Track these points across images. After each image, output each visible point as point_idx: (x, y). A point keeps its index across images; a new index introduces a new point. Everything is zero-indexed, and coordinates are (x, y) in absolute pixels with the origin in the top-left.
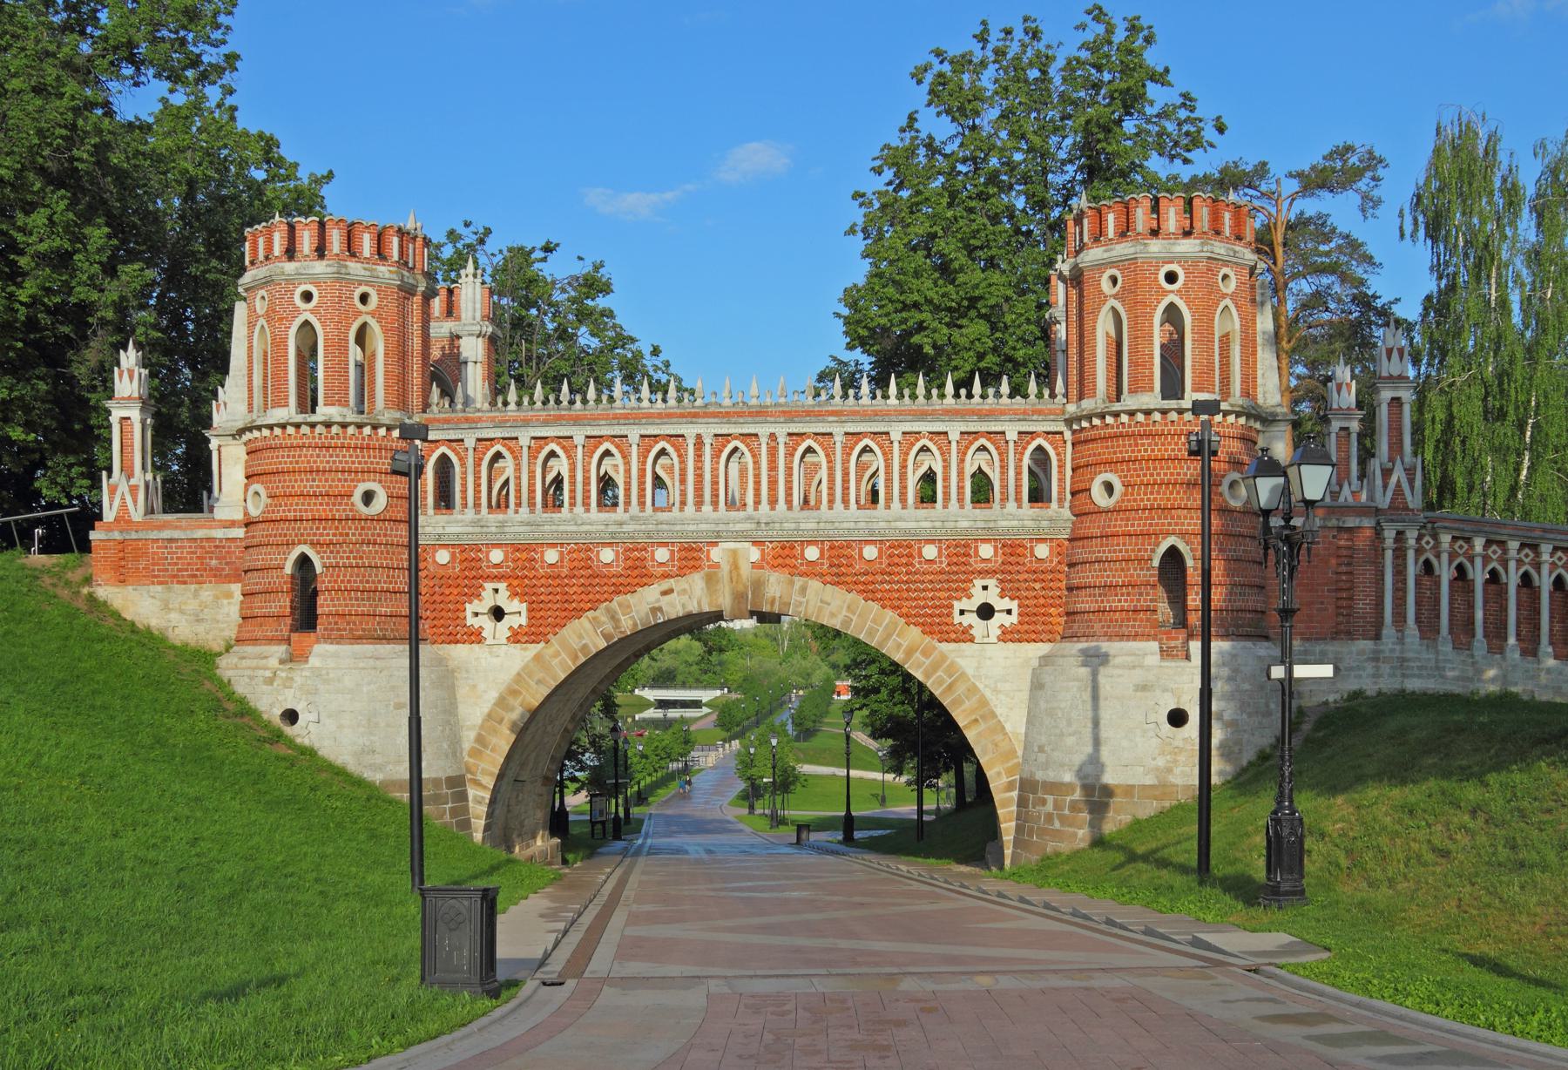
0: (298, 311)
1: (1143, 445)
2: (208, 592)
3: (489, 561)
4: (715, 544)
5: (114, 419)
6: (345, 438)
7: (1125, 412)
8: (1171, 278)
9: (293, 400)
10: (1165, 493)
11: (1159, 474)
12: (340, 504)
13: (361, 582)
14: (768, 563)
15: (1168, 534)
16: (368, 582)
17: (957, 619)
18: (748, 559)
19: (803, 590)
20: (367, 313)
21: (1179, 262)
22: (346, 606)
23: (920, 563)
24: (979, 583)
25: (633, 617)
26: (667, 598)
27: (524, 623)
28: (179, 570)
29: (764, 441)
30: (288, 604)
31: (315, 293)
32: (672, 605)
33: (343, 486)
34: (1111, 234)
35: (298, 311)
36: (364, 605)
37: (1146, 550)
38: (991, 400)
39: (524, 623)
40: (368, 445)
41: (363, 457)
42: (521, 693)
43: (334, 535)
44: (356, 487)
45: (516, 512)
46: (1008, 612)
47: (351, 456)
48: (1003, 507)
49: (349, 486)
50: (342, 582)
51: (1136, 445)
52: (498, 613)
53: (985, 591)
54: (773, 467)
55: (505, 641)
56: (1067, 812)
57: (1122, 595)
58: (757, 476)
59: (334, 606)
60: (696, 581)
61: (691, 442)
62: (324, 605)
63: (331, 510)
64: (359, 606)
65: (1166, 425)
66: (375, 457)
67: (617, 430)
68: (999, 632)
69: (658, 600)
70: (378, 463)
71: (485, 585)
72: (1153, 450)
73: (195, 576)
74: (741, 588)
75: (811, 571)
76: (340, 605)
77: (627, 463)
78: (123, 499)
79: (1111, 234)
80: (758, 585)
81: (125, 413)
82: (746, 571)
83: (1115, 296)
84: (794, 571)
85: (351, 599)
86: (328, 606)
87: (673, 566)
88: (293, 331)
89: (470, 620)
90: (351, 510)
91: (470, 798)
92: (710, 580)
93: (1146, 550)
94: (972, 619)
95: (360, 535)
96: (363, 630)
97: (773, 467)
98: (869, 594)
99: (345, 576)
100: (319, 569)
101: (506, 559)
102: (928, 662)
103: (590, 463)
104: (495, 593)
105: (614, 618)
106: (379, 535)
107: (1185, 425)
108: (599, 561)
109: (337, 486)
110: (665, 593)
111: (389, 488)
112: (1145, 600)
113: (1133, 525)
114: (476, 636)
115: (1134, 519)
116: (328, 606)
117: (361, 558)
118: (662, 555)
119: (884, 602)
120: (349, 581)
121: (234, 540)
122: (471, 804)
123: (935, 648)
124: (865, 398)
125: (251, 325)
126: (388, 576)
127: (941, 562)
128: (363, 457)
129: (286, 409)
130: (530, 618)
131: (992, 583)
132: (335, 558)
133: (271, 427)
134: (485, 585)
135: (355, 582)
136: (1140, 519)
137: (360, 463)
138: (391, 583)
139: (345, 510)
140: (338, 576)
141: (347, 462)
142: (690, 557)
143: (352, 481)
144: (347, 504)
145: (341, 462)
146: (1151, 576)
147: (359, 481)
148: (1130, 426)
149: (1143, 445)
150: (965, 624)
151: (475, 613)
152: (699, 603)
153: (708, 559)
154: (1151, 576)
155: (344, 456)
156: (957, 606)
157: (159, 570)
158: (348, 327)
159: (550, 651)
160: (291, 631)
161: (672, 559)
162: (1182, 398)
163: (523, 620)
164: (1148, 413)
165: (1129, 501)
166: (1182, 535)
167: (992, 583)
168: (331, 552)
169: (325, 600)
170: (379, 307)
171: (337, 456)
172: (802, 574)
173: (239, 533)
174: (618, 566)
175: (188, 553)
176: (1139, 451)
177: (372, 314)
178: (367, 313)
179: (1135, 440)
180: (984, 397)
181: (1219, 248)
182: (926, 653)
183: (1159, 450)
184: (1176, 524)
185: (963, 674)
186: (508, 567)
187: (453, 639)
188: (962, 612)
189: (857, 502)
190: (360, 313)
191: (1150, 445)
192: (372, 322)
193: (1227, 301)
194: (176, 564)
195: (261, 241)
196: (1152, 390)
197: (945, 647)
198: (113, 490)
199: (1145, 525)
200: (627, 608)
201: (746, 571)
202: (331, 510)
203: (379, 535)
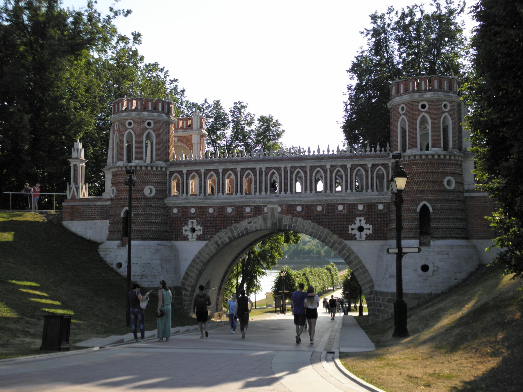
0: (127, 129)
1: (413, 168)
2: (99, 222)
3: (190, 212)
4: (266, 206)
5: (72, 165)
6: (141, 171)
7: (407, 156)
8: (423, 106)
9: (125, 158)
10: (421, 185)
11: (419, 178)
12: (139, 193)
13: (146, 219)
14: (284, 212)
15: (422, 201)
16: (148, 219)
17: (350, 232)
18: (277, 211)
19: (296, 222)
20: (150, 129)
21: (426, 101)
22: (140, 227)
23: (337, 212)
24: (358, 219)
25: (238, 231)
26: (250, 225)
27: (202, 234)
28: (90, 215)
29: (283, 169)
30: (121, 227)
31: (133, 125)
32: (251, 227)
33: (140, 187)
34: (402, 91)
35: (127, 129)
36: (147, 228)
37: (415, 206)
38: (373, 152)
39: (202, 234)
40: (149, 173)
41: (147, 177)
42: (200, 258)
43: (137, 203)
44: (145, 187)
45: (236, 194)
46: (368, 229)
47: (143, 177)
48: (366, 191)
49: (142, 187)
50: (139, 219)
51: (411, 168)
52: (361, 229)
53: (360, 221)
54: (286, 178)
55: (364, 240)
56: (386, 303)
57: (407, 223)
58: (255, 181)
59: (136, 228)
60: (260, 218)
61: (283, 169)
62: (134, 227)
63: (136, 195)
64: (145, 228)
65: (422, 160)
66: (152, 177)
67: (233, 167)
68: (365, 237)
69: (247, 225)
70: (152, 179)
71: (189, 220)
72: (417, 170)
73: (95, 217)
74: (275, 221)
75: (299, 215)
76: (138, 227)
77: (280, 177)
78: (74, 192)
79: (402, 91)
80: (281, 220)
81: (75, 163)
82: (277, 215)
83: (403, 114)
84: (294, 215)
85: (142, 225)
86: (134, 228)
87: (252, 213)
88: (125, 136)
89: (184, 232)
90: (143, 195)
91: (183, 294)
92: (265, 219)
93: (415, 206)
94: (356, 232)
95: (146, 203)
96: (146, 236)
97: (286, 178)
98: (319, 223)
99: (140, 217)
100: (431, 210)
101: (196, 212)
102: (340, 247)
103: (373, 174)
104: (192, 223)
105: (231, 231)
106: (153, 203)
107: (411, 161)
108: (227, 212)
109: (138, 187)
110: (249, 223)
111: (156, 187)
112: (415, 225)
113: (410, 197)
114: (353, 238)
115: (411, 195)
116: (134, 228)
117: (146, 211)
118: (248, 210)
119: (325, 226)
120: (142, 219)
121: (108, 205)
122: (183, 297)
123: (343, 242)
124: (368, 151)
125: (114, 133)
126: (155, 217)
127: (345, 211)
128: (147, 177)
129: (123, 162)
130: (203, 232)
131: (362, 218)
132: (137, 211)
133: (118, 167)
134: (189, 220)
135: (144, 219)
136: (413, 195)
137: (146, 179)
138: (156, 220)
139: (141, 195)
140: (138, 217)
141: (142, 179)
142: (258, 210)
143: (144, 185)
144: (142, 193)
145: (140, 179)
146: (417, 215)
147: (146, 185)
148: (409, 161)
149: (413, 168)
150: (353, 234)
151: (186, 230)
152: (261, 226)
153: (264, 211)
154: (417, 215)
155: (141, 177)
156: (350, 227)
157: (84, 216)
158: (143, 134)
159: (211, 243)
160: (122, 236)
161: (251, 211)
162: (398, 150)
163: (201, 233)
164: (415, 156)
165: (409, 188)
166: (428, 200)
167: (362, 218)
168: (136, 209)
169: (134, 225)
170: (154, 126)
171: (139, 177)
172: (297, 216)
173: (109, 203)
174: (233, 214)
175: (93, 210)
176: (412, 170)
177: (151, 129)
178: (150, 129)
179: (411, 166)
180: (371, 151)
181: (441, 95)
182: (339, 244)
183: (419, 169)
184: (426, 197)
185: (353, 252)
186: (197, 214)
187: (176, 239)
188: (352, 229)
189: (377, 188)
190: (147, 129)
191: (416, 167)
192: (152, 132)
193: (446, 114)
194: (89, 213)
195: (116, 106)
196: (417, 147)
197: (347, 242)
198: (70, 189)
199: (414, 197)
200: (236, 228)
201: (277, 215)
202: (136, 195)
203: (153, 203)
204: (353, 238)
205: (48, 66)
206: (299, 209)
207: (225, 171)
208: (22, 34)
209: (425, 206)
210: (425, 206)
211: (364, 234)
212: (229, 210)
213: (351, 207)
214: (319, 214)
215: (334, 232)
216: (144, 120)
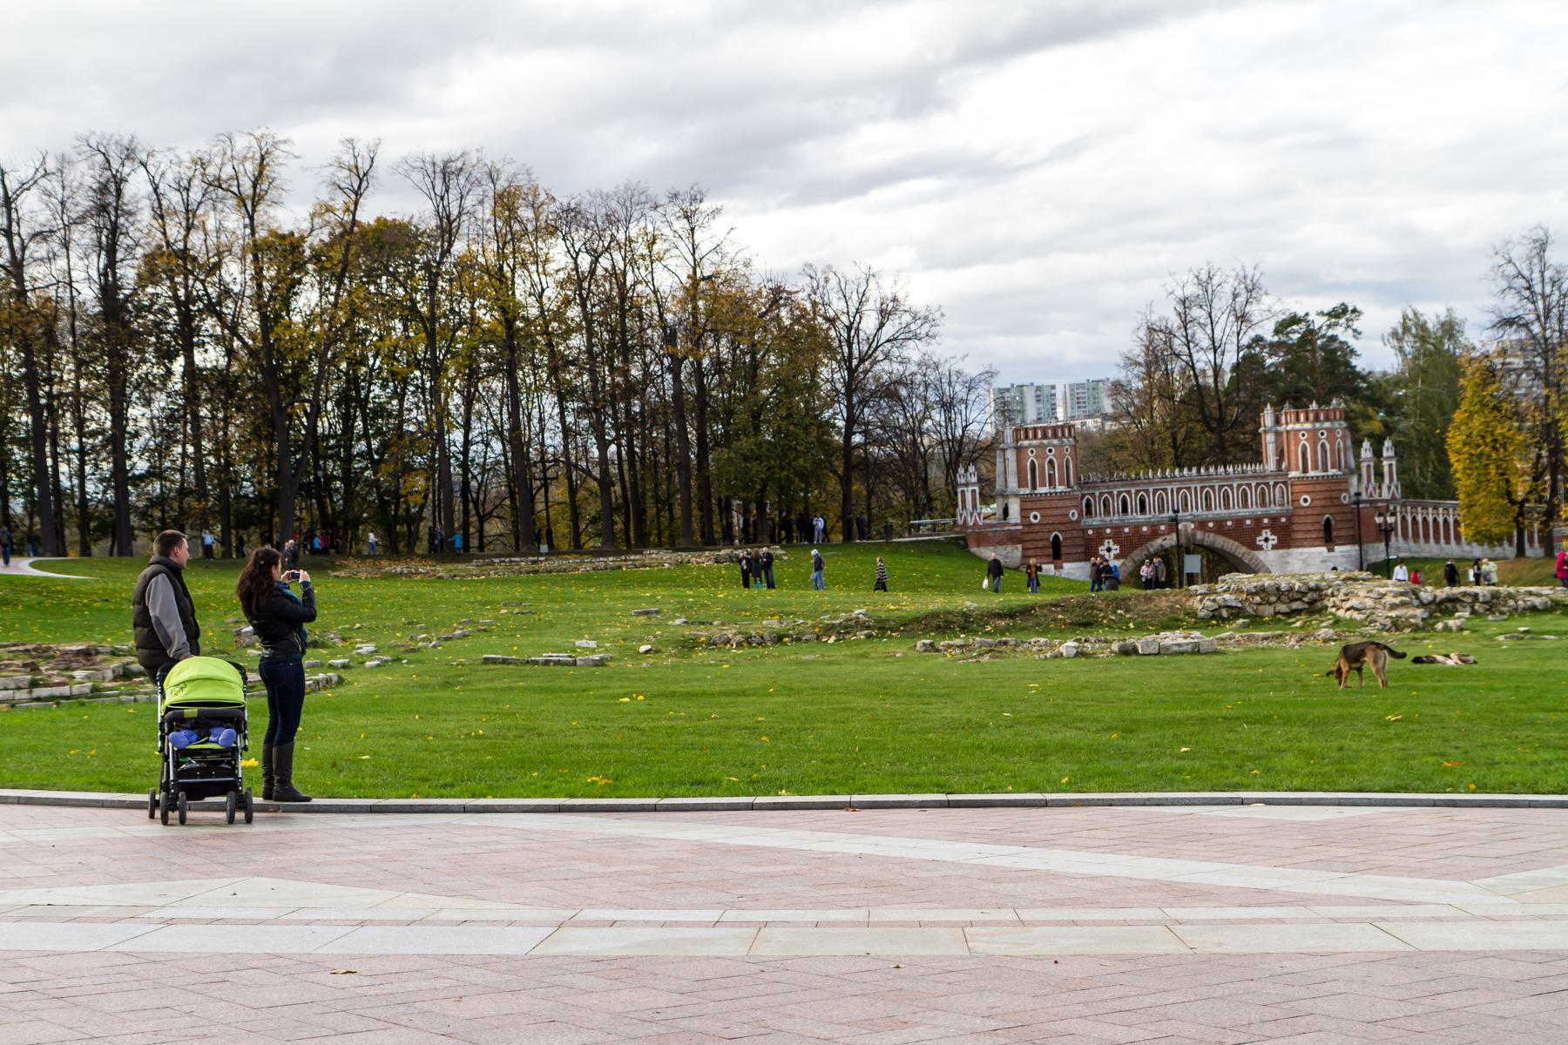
46: (1274, 540)
52: (1266, 540)
53: (1266, 533)
62: (1064, 550)
75: (1211, 530)
114: (1260, 548)
204: (1260, 548)
205: (159, 439)
206: (1211, 525)
207: (1276, 484)
208: (99, 416)
209: (1056, 536)
210: (1056, 536)
211: (1112, 553)
212: (1145, 529)
213: (1258, 520)
214: (1230, 529)
215: (1243, 544)
216: (1046, 446)
